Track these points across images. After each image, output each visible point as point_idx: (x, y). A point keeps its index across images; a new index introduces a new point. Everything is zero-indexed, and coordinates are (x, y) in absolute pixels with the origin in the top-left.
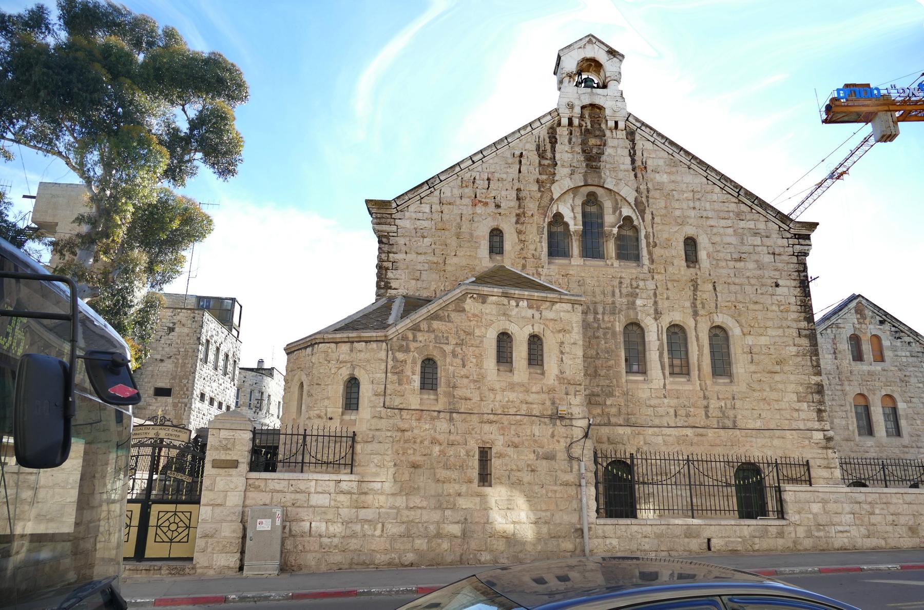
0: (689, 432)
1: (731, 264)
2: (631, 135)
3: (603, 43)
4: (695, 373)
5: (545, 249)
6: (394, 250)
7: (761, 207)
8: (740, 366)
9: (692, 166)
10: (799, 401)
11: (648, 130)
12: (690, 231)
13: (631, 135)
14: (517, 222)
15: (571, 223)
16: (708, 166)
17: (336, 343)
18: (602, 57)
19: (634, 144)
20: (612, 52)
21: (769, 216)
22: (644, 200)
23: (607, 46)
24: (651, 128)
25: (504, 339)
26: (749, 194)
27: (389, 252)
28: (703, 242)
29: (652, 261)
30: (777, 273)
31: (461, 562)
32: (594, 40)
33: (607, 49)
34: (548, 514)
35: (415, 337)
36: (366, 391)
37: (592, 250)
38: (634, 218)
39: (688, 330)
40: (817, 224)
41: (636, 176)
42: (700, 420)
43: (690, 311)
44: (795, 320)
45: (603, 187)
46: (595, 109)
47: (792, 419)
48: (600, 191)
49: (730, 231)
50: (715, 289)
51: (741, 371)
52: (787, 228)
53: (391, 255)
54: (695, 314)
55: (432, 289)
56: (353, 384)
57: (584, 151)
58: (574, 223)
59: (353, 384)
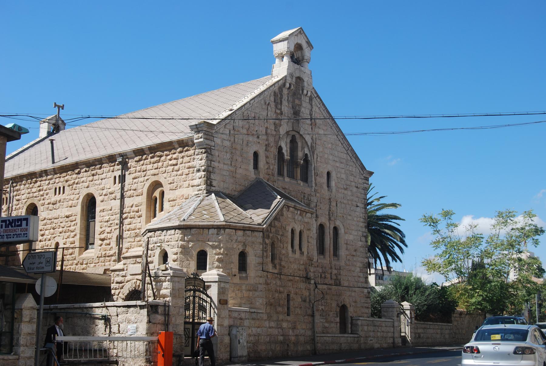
0: (325, 287)
1: (343, 191)
2: (311, 99)
3: (306, 36)
4: (327, 254)
5: (277, 170)
6: (214, 159)
7: (355, 159)
8: (343, 252)
9: (333, 128)
10: (360, 272)
11: (319, 100)
12: (330, 168)
13: (311, 99)
14: (266, 150)
15: (285, 154)
16: (340, 129)
17: (236, 230)
18: (304, 45)
19: (312, 107)
20: (308, 43)
21: (357, 165)
22: (314, 145)
23: (308, 39)
24: (321, 100)
25: (293, 231)
26: (352, 150)
27: (211, 161)
28: (333, 175)
29: (316, 185)
30: (357, 199)
31: (394, 347)
32: (302, 32)
33: (307, 40)
34: (304, 331)
35: (271, 230)
36: (252, 260)
37: (292, 176)
38: (309, 155)
39: (325, 226)
40: (373, 173)
41: (312, 128)
42: (328, 281)
43: (327, 217)
44: (361, 227)
45: (299, 133)
46: (299, 79)
47: (358, 282)
48: (297, 136)
49: (343, 171)
50: (337, 205)
51: (343, 254)
52: (362, 173)
53: (213, 162)
54: (330, 219)
55: (230, 189)
56: (243, 256)
57: (293, 107)
58: (287, 157)
59: (243, 256)
